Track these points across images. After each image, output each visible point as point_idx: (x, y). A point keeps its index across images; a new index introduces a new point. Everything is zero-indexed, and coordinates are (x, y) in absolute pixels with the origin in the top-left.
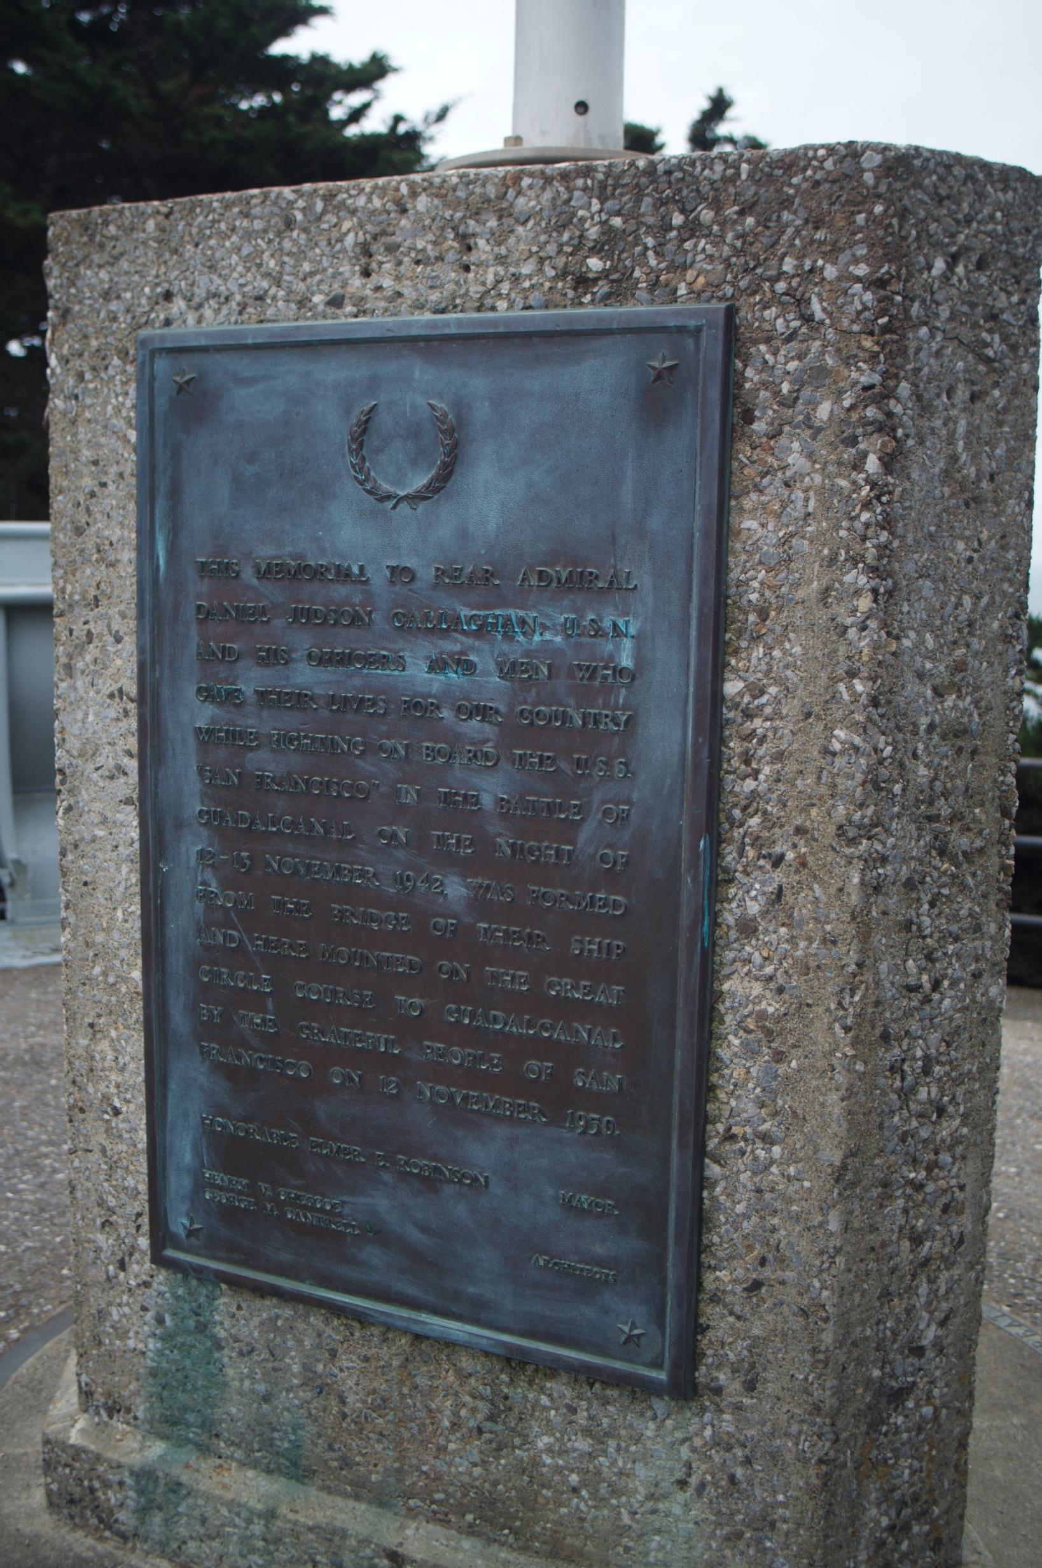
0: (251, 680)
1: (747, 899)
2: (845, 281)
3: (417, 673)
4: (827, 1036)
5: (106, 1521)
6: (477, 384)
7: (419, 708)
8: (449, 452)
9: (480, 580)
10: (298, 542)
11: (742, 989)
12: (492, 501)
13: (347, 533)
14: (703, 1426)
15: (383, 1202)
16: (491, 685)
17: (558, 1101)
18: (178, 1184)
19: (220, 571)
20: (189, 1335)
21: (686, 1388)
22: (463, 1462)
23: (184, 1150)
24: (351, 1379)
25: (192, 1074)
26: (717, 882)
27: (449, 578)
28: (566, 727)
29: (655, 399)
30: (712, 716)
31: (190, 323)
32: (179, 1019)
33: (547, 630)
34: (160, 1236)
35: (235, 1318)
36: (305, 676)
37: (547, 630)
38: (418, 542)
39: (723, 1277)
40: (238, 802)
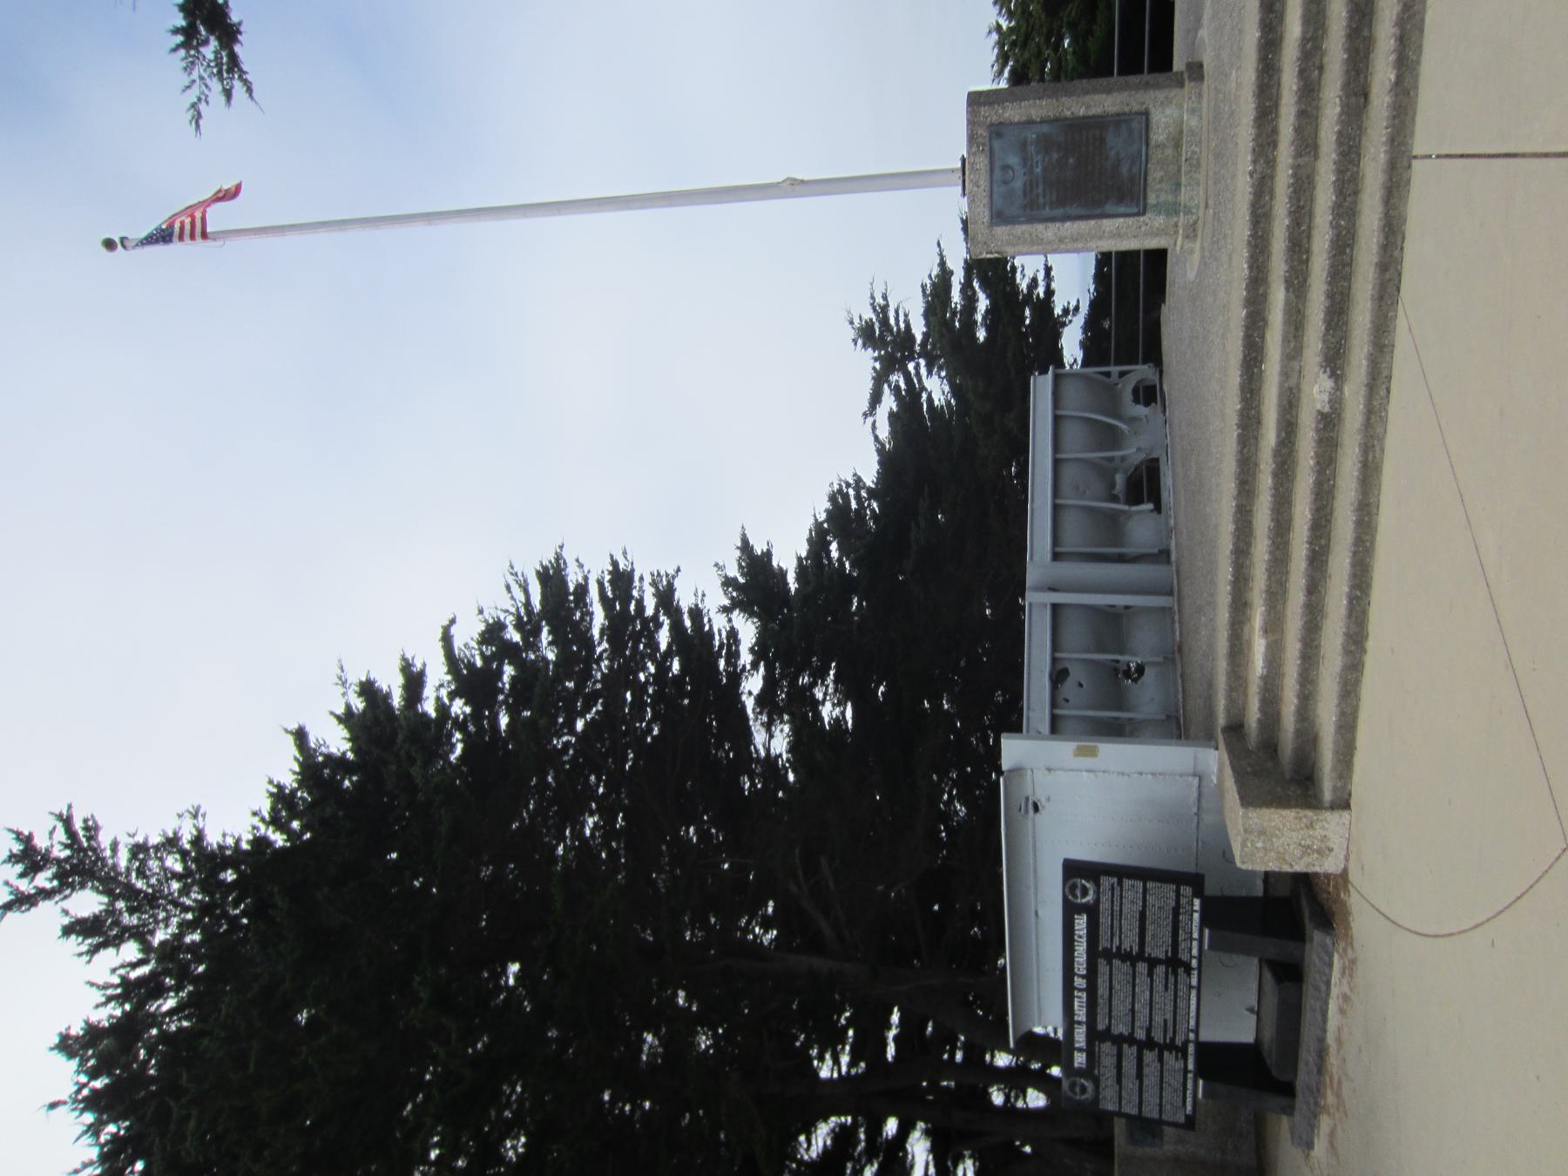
0: (1041, 200)
1: (1068, 114)
2: (983, 110)
3: (1039, 170)
4: (1087, 98)
5: (1196, 222)
6: (998, 164)
7: (1044, 169)
8: (1006, 168)
9: (1025, 161)
10: (1020, 193)
11: (1082, 112)
12: (1014, 160)
13: (1018, 184)
14: (1153, 110)
15: (1124, 169)
16: (1040, 157)
17: (1102, 140)
18: (1129, 210)
19: (1025, 207)
20: (1158, 208)
21: (1146, 114)
22: (1169, 151)
23: (1122, 209)
24: (1159, 175)
25: (1109, 208)
26: (1066, 118)
27: (1025, 166)
28: (1045, 144)
29: (999, 135)
30: (1043, 122)
31: (986, 219)
32: (1098, 211)
33: (1031, 149)
34: (1138, 214)
35: (1152, 199)
36: (1040, 190)
37: (1031, 149)
38: (1020, 171)
39: (1127, 109)
40: (1061, 202)
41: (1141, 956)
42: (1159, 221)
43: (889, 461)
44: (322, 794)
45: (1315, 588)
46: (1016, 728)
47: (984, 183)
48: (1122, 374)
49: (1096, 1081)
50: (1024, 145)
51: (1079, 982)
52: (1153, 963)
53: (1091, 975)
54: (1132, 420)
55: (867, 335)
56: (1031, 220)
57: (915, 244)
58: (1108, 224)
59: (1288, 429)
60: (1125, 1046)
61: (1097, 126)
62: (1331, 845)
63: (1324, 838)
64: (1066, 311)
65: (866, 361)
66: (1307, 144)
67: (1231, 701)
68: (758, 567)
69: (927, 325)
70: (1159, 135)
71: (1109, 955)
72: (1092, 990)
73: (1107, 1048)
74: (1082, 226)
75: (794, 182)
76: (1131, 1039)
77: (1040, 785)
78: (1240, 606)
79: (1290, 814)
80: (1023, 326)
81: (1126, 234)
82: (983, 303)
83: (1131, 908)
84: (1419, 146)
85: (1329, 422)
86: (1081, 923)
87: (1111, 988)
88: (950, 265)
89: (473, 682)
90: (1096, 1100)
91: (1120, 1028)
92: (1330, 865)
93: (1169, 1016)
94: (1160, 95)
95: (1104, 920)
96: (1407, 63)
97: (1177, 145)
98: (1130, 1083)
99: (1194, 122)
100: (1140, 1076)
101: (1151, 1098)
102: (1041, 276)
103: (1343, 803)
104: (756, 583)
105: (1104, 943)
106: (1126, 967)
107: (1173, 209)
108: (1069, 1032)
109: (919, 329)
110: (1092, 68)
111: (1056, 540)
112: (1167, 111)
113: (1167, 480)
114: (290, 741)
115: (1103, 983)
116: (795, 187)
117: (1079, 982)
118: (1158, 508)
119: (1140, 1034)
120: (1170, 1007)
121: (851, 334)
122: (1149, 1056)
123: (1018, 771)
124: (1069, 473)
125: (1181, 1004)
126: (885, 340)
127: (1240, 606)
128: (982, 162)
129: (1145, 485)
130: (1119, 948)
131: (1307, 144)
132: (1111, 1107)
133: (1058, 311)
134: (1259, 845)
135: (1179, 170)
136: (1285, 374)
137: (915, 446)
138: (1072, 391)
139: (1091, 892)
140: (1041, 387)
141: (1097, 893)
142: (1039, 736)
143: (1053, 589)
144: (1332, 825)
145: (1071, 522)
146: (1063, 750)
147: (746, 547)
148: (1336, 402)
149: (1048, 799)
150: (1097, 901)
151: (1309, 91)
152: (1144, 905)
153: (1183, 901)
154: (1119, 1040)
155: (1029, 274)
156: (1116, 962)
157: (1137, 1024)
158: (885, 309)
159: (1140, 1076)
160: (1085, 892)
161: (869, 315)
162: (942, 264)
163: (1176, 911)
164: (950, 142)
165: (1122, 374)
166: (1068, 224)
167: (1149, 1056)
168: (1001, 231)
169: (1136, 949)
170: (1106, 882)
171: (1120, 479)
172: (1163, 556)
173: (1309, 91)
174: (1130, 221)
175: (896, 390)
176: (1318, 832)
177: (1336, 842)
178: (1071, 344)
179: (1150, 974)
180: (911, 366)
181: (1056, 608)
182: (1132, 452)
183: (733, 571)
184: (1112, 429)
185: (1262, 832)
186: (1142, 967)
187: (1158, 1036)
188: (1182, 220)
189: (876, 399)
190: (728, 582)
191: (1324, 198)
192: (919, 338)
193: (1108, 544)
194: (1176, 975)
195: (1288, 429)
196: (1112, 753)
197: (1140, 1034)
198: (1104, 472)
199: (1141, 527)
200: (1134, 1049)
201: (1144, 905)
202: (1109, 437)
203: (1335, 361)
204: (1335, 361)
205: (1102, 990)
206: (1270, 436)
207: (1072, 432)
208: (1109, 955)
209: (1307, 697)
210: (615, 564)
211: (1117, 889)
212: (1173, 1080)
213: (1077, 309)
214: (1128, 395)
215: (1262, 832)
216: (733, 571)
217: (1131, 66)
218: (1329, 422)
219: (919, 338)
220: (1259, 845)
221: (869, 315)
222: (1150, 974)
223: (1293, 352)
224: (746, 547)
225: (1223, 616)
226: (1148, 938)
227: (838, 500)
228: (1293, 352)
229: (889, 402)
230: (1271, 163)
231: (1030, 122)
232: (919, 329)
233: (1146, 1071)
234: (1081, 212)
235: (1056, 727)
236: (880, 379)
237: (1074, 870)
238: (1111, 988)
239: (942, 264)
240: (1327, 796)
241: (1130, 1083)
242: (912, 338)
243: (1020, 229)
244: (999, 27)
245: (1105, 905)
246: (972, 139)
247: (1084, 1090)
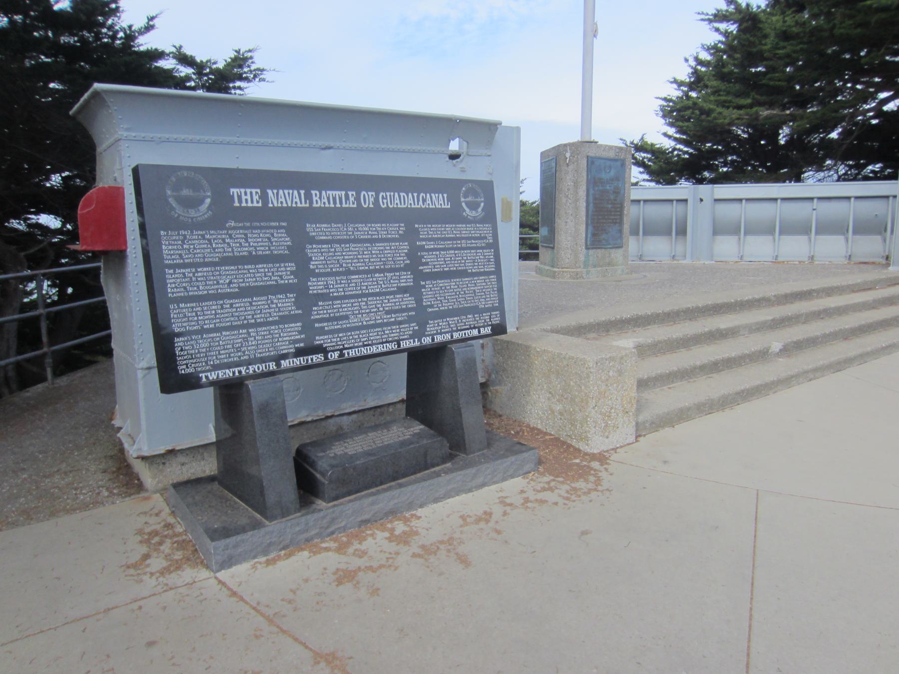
20: (587, 256)
23: (589, 235)
25: (590, 228)
31: (590, 154)
35: (591, 252)
41: (419, 276)
49: (216, 222)
51: (368, 198)
52: (415, 291)
53: (378, 215)
55: (239, 61)
60: (291, 266)
62: (611, 436)
63: (616, 427)
71: (411, 235)
73: (282, 241)
76: (304, 271)
86: (439, 201)
87: (372, 241)
91: (317, 258)
93: (354, 321)
95: (449, 230)
98: (228, 278)
99: (619, 272)
100: (246, 292)
105: (426, 231)
106: (402, 260)
117: (368, 198)
119: (316, 286)
120: (365, 320)
125: (374, 335)
130: (422, 249)
134: (611, 374)
135: (601, 266)
139: (474, 214)
141: (474, 221)
149: (454, 165)
150: (466, 221)
152: (473, 275)
153: (486, 316)
154: (298, 256)
156: (405, 247)
157: (331, 281)
159: (246, 292)
160: (473, 206)
163: (475, 310)
166: (585, 204)
168: (584, 163)
169: (426, 269)
171: (355, 582)
174: (584, 241)
175: (188, 78)
179: (403, 290)
185: (620, 373)
186: (407, 279)
187: (319, 311)
194: (410, 320)
200: (292, 280)
201: (473, 275)
203: (788, 350)
205: (364, 230)
208: (411, 235)
211: (480, 243)
215: (620, 373)
220: (611, 374)
222: (403, 290)
226: (441, 283)
229: (185, 71)
233: (260, 301)
234: (590, 212)
236: (200, 68)
238: (372, 241)
241: (228, 278)
245: (464, 230)
247: (193, 203)
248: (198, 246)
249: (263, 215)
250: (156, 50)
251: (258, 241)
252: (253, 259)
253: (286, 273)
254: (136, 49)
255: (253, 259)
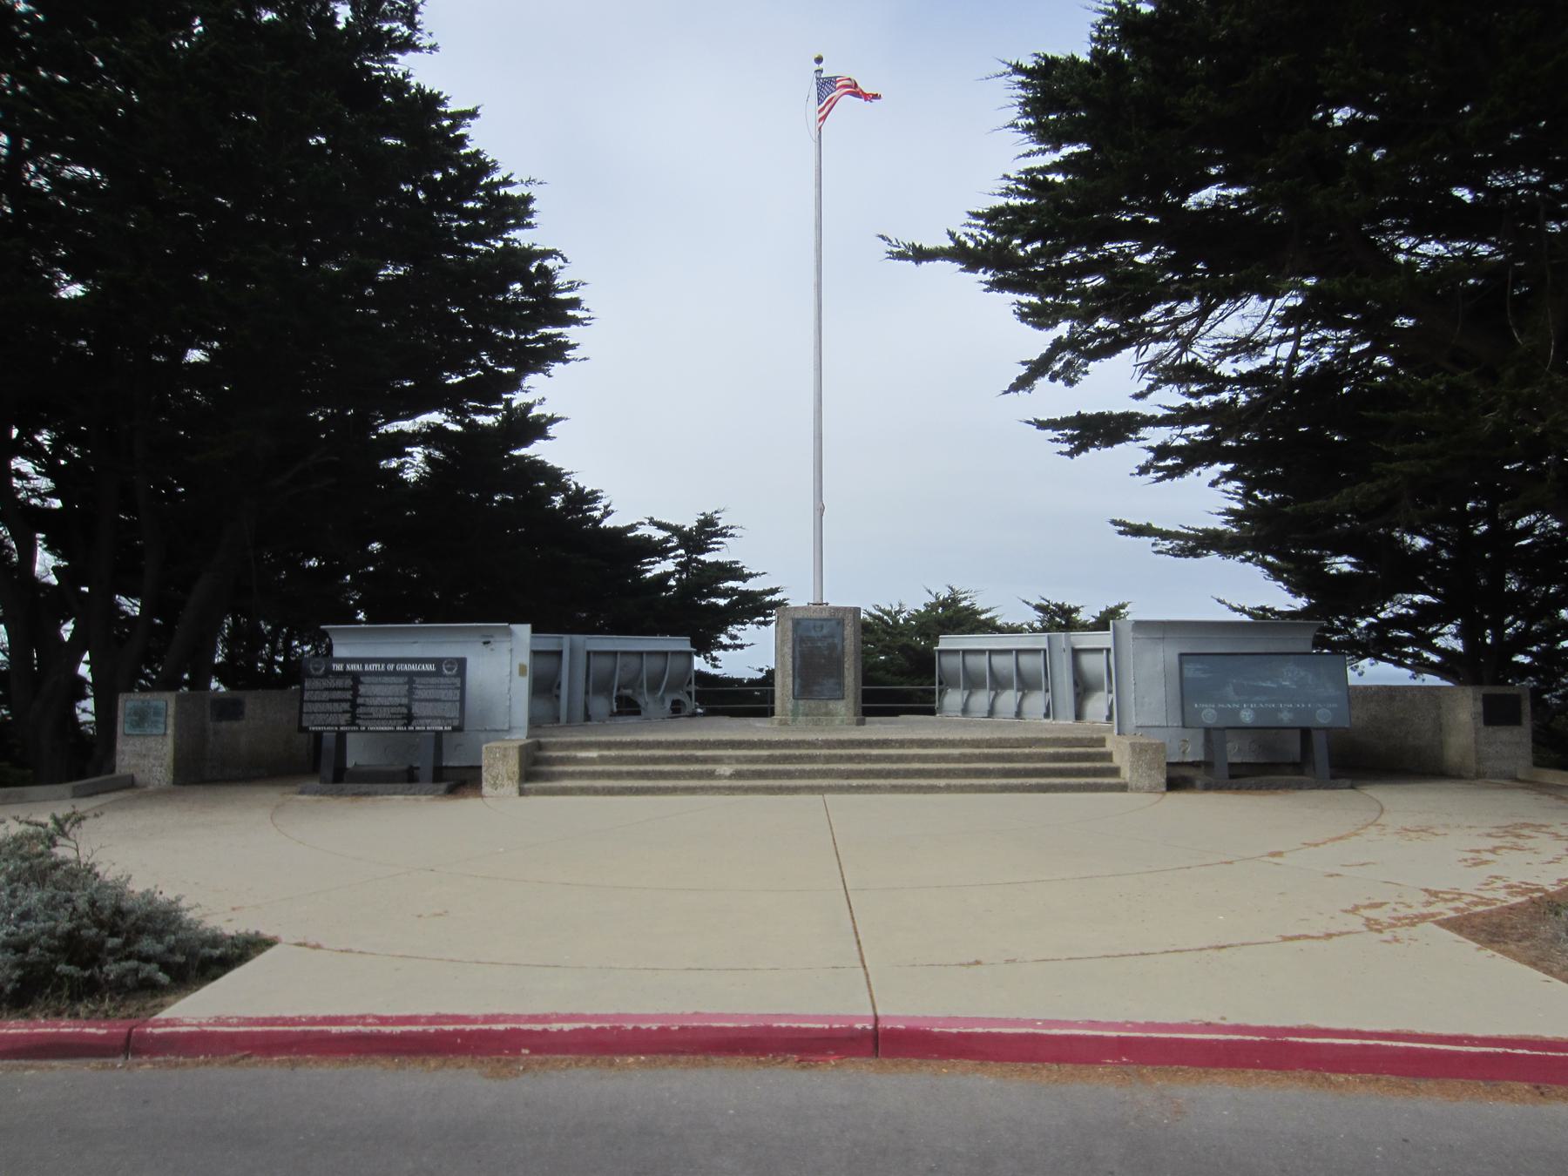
12: (825, 631)
13: (813, 634)
20: (796, 707)
28: (832, 647)
35: (801, 702)
40: (803, 655)
42: (789, 706)
43: (618, 534)
44: (426, 125)
45: (630, 775)
46: (534, 631)
47: (815, 615)
48: (689, 694)
50: (832, 636)
51: (391, 667)
53: (395, 673)
54: (662, 700)
56: (794, 641)
57: (764, 553)
58: (790, 680)
59: (705, 760)
61: (838, 673)
64: (715, 659)
65: (689, 523)
66: (828, 759)
67: (555, 744)
68: (537, 428)
69: (710, 564)
70: (832, 705)
72: (386, 673)
73: (349, 682)
74: (789, 666)
75: (822, 510)
76: (356, 694)
77: (502, 647)
78: (609, 745)
79: (516, 769)
80: (706, 628)
81: (783, 689)
82: (722, 602)
83: (442, 694)
84: (828, 797)
85: (711, 775)
86: (430, 668)
88: (751, 581)
89: (517, 262)
90: (310, 676)
91: (362, 689)
92: (486, 789)
94: (851, 705)
95: (433, 680)
96: (858, 789)
97: (826, 714)
98: (325, 696)
100: (331, 701)
101: (317, 707)
102: (738, 642)
103: (522, 793)
104: (531, 427)
105: (418, 680)
107: (795, 713)
108: (340, 660)
109: (707, 558)
110: (868, 674)
111: (597, 653)
112: (844, 708)
113: (632, 720)
114: (470, 107)
115: (393, 679)
116: (820, 510)
117: (391, 667)
118: (612, 714)
119: (360, 701)
121: (709, 512)
122: (346, 706)
123: (510, 633)
124: (634, 661)
126: (705, 532)
127: (609, 745)
128: (825, 615)
129: (628, 707)
131: (828, 759)
132: (307, 684)
133: (715, 653)
136: (730, 757)
137: (628, 549)
138: (679, 663)
140: (683, 644)
142: (532, 644)
143: (571, 650)
144: (511, 788)
145: (606, 663)
146: (525, 659)
147: (553, 420)
148: (720, 777)
151: (850, 759)
154: (355, 689)
155: (739, 634)
158: (725, 535)
159: (331, 701)
161: (721, 524)
162: (751, 575)
164: (837, 599)
165: (689, 694)
167: (346, 706)
168: (790, 624)
170: (458, 681)
171: (629, 692)
172: (588, 718)
173: (850, 759)
175: (667, 540)
176: (506, 782)
177: (501, 791)
178: (699, 664)
180: (681, 552)
181: (559, 654)
182: (645, 699)
183: (535, 411)
184: (658, 687)
187: (360, 710)
188: (790, 718)
189: (661, 526)
190: (529, 407)
191: (807, 767)
192: (702, 557)
193: (599, 686)
195: (705, 760)
196: (523, 686)
197: (360, 701)
198: (633, 682)
199: (601, 705)
202: (654, 686)
203: (738, 775)
204: (738, 775)
205: (386, 679)
206: (700, 753)
207: (657, 663)
209: (572, 775)
210: (573, 347)
212: (332, 719)
213: (715, 666)
214: (676, 696)
216: (535, 411)
217: (867, 696)
218: (711, 775)
219: (702, 557)
221: (721, 524)
223: (738, 760)
224: (553, 420)
225: (604, 738)
227: (593, 497)
228: (738, 760)
229: (659, 535)
230: (821, 747)
231: (843, 640)
232: (707, 558)
235: (535, 654)
236: (676, 530)
237: (462, 663)
239: (751, 575)
240: (527, 785)
241: (325, 696)
242: (702, 553)
243: (790, 634)
244: (900, 612)
245: (442, 680)
246: (837, 609)
248: (317, 683)
249: (344, 673)
250: (542, 462)
251: (339, 683)
252: (336, 689)
253: (348, 695)
254: (1352, 560)
255: (336, 689)
